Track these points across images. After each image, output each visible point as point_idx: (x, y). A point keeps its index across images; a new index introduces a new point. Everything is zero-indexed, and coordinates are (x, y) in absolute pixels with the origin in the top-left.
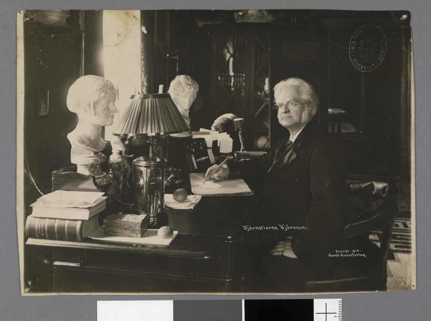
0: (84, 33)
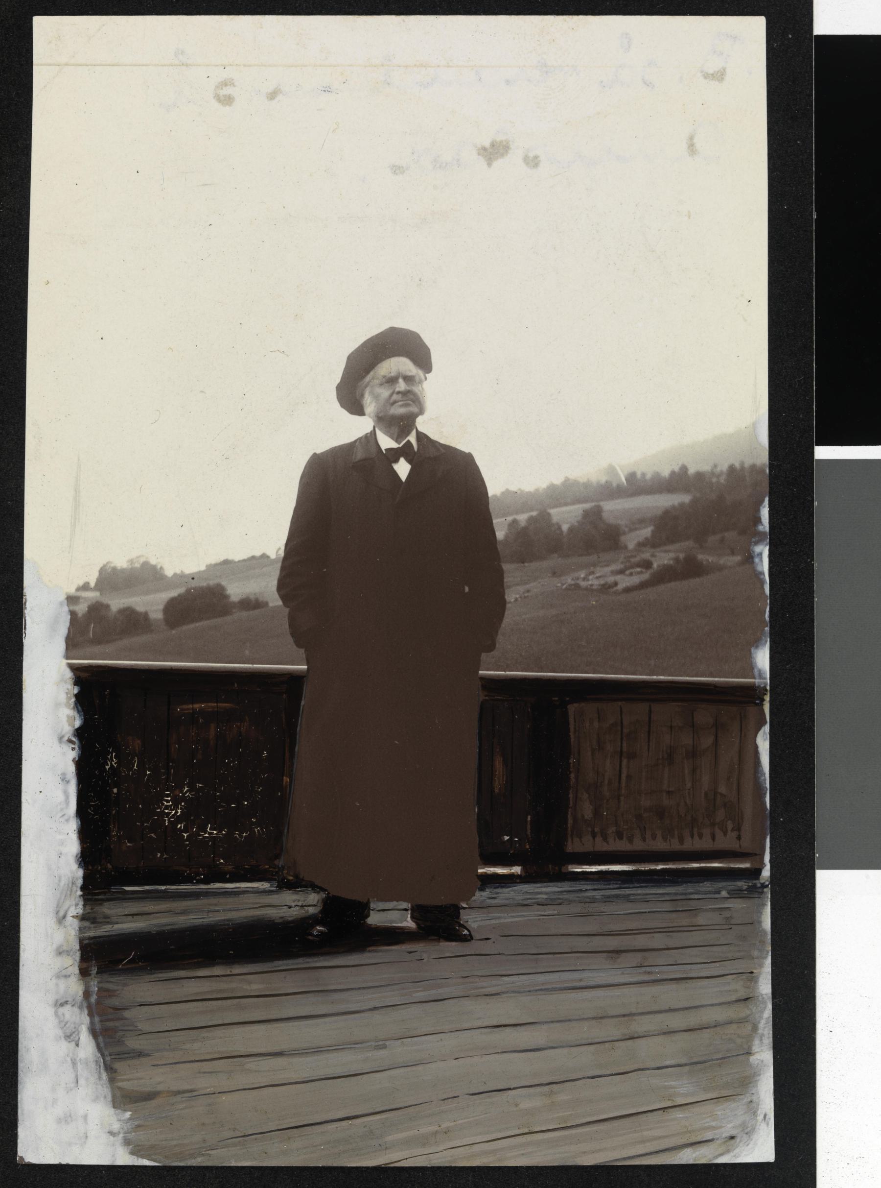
0: (823, 453)
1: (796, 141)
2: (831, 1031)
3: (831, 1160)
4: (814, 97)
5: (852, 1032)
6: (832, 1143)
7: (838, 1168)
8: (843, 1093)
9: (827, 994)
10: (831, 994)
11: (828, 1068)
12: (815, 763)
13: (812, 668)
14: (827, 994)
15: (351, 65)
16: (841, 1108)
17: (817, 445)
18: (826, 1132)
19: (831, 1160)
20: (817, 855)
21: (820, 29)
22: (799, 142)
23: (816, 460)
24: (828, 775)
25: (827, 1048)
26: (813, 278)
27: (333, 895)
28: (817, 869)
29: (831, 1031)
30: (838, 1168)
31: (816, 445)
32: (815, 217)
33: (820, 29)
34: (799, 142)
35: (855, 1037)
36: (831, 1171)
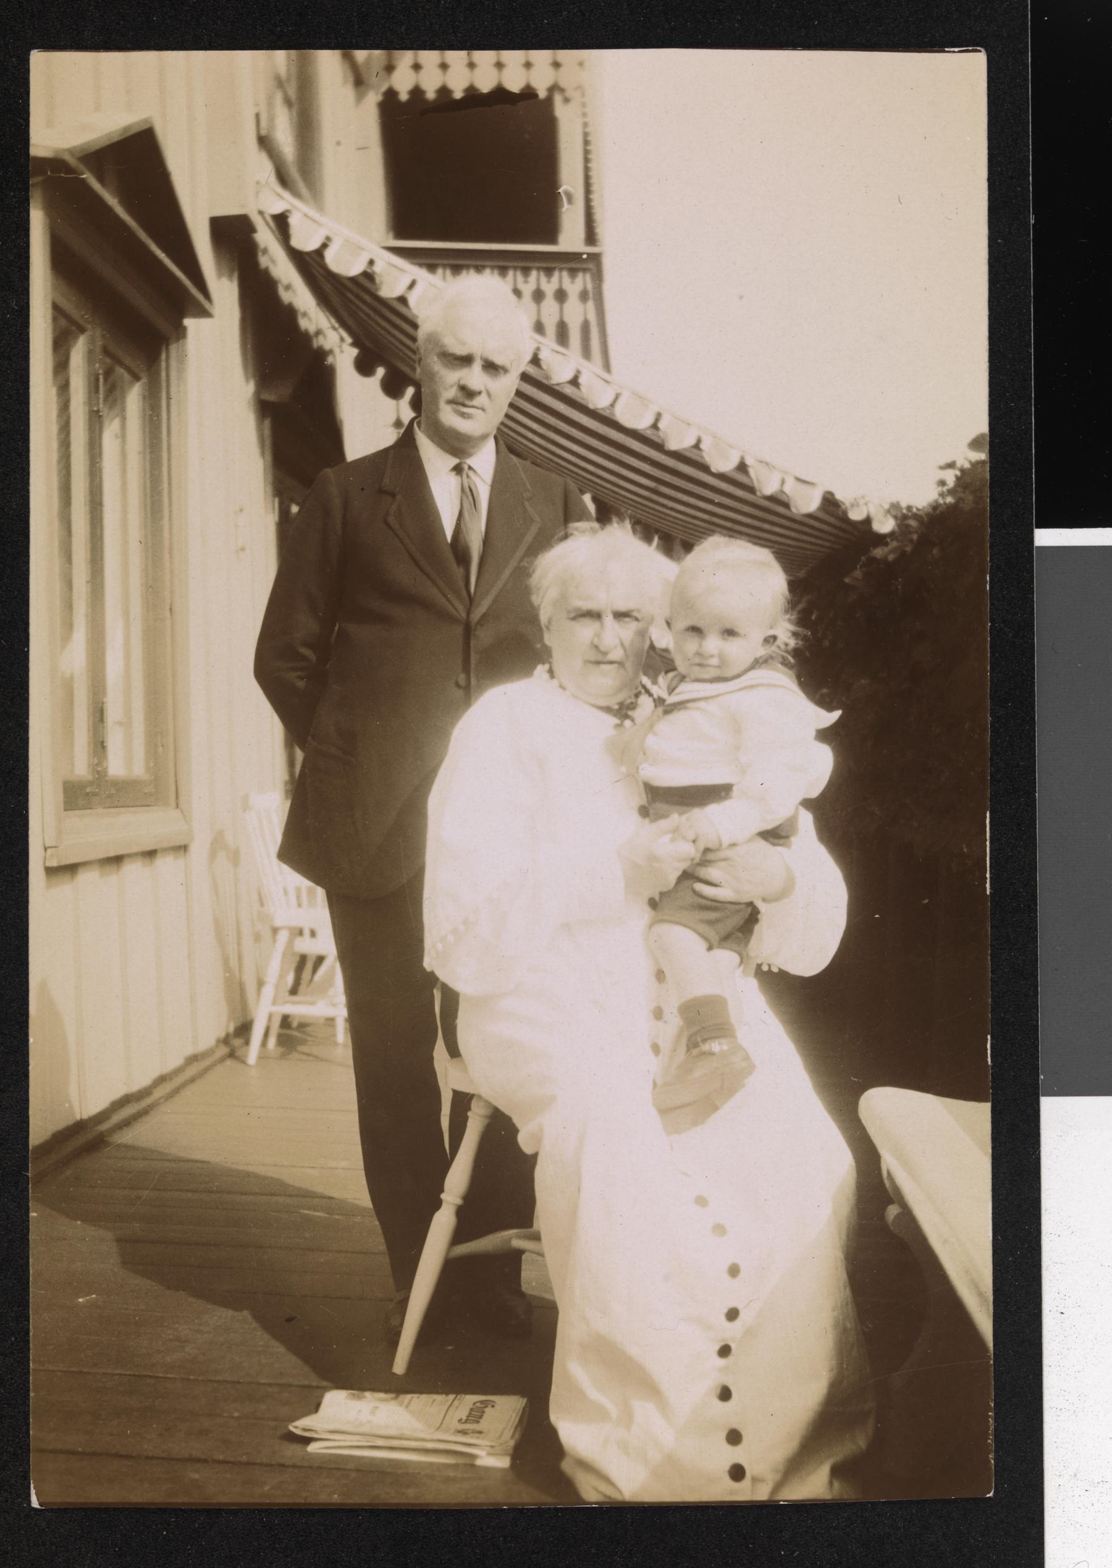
0: (1046, 537)
1: (997, 240)
2: (1062, 1313)
3: (1063, 1485)
4: (1030, 60)
5: (1090, 1314)
6: (1064, 1463)
7: (1073, 1496)
8: (1080, 1395)
9: (1056, 1263)
10: (1062, 1263)
11: (1059, 1362)
12: (1037, 754)
13: (1030, 501)
14: (1056, 1263)
15: (767, 464)
16: (1077, 1416)
17: (1038, 527)
18: (1057, 1447)
19: (1063, 1485)
20: (1042, 1077)
21: (38, 59)
22: (1000, 241)
23: (1039, 548)
24: (1056, 969)
25: (1056, 1336)
26: (1029, 155)
27: (780, 970)
28: (1042, 1096)
29: (1062, 1313)
30: (1073, 1496)
31: (1036, 528)
32: (1032, 221)
33: (38, 59)
34: (1000, 241)
35: (1095, 1320)
36: (1063, 1500)
